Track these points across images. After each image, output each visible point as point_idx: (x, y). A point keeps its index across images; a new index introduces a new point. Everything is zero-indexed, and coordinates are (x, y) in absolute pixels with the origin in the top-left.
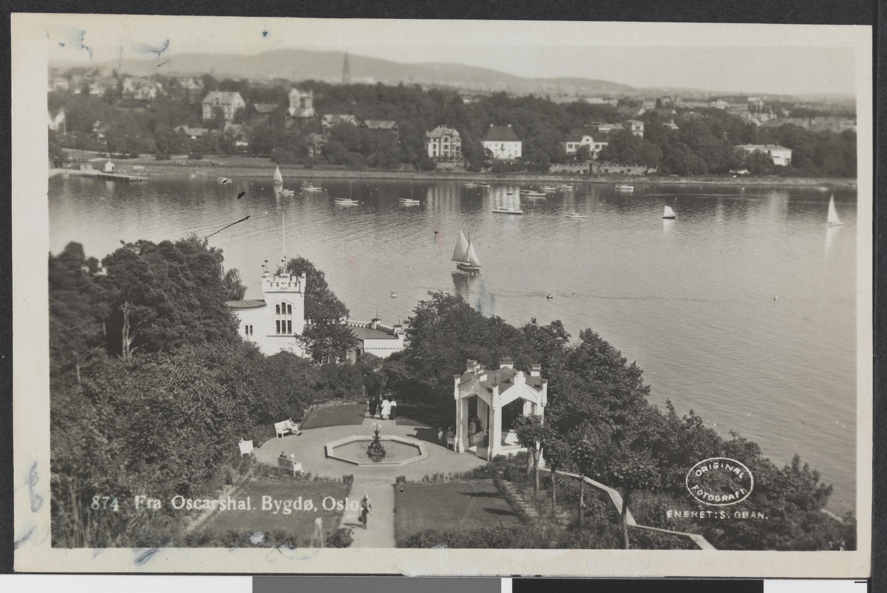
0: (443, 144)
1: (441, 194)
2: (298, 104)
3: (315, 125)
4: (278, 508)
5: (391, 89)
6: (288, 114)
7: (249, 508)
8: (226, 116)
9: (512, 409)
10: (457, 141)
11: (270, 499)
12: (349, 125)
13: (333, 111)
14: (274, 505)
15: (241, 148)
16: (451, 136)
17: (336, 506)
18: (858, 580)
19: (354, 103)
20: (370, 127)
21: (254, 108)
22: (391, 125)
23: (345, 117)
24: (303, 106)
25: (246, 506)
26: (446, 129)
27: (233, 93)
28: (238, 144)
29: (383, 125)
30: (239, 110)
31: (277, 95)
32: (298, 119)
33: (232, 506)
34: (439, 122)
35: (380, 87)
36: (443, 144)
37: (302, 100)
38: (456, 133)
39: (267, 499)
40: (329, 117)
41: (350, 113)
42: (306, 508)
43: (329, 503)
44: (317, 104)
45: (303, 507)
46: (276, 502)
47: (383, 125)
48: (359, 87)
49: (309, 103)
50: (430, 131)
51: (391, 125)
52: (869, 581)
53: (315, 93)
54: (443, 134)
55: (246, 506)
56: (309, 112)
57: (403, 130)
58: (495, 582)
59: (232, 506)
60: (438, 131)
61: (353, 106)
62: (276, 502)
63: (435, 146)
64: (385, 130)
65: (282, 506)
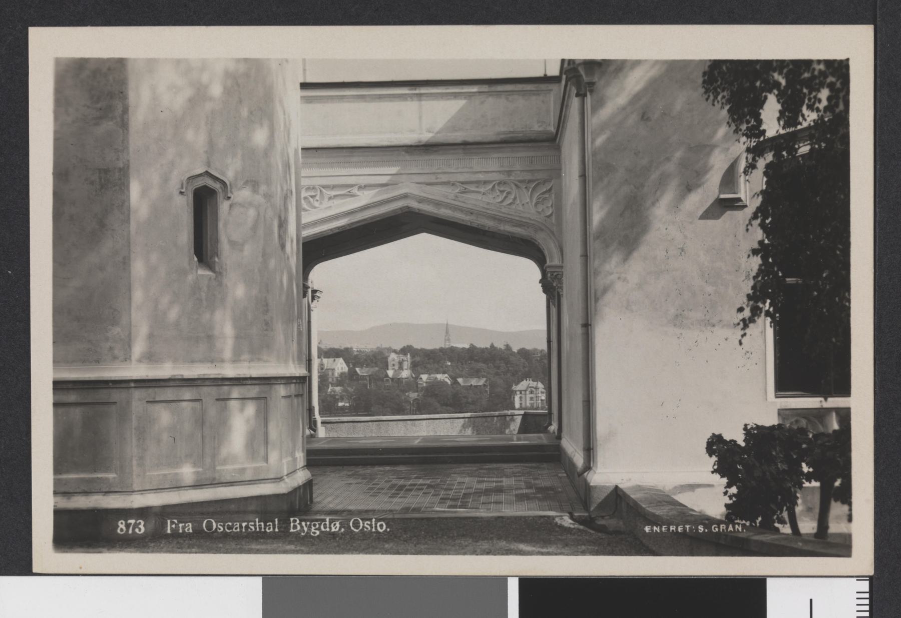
0: (529, 396)
1: (431, 118)
2: (397, 367)
3: (412, 384)
4: (306, 529)
5: (483, 350)
6: (387, 376)
7: (277, 530)
8: (330, 380)
9: (842, 131)
10: (542, 392)
11: (298, 521)
12: (443, 383)
13: (428, 372)
14: (302, 527)
15: (343, 408)
16: (536, 388)
17: (364, 527)
18: (859, 578)
19: (449, 364)
20: (462, 384)
21: (356, 372)
22: (482, 382)
23: (440, 377)
24: (401, 368)
25: (274, 528)
26: (531, 382)
27: (337, 359)
28: (340, 404)
29: (474, 382)
30: (342, 374)
31: (378, 359)
32: (397, 381)
33: (260, 528)
34: (526, 376)
35: (473, 348)
36: (529, 396)
37: (401, 364)
38: (540, 385)
39: (295, 521)
40: (425, 377)
41: (444, 373)
42: (333, 530)
43: (356, 525)
44: (414, 366)
45: (330, 528)
46: (303, 524)
47: (474, 382)
48: (452, 350)
49: (406, 365)
50: (517, 384)
51: (482, 382)
52: (871, 579)
53: (413, 357)
54: (528, 387)
55: (274, 528)
56: (405, 374)
57: (493, 385)
58: (502, 581)
59: (260, 528)
60: (523, 385)
61: (447, 366)
62: (303, 524)
63: (521, 398)
64: (476, 386)
65: (310, 527)
